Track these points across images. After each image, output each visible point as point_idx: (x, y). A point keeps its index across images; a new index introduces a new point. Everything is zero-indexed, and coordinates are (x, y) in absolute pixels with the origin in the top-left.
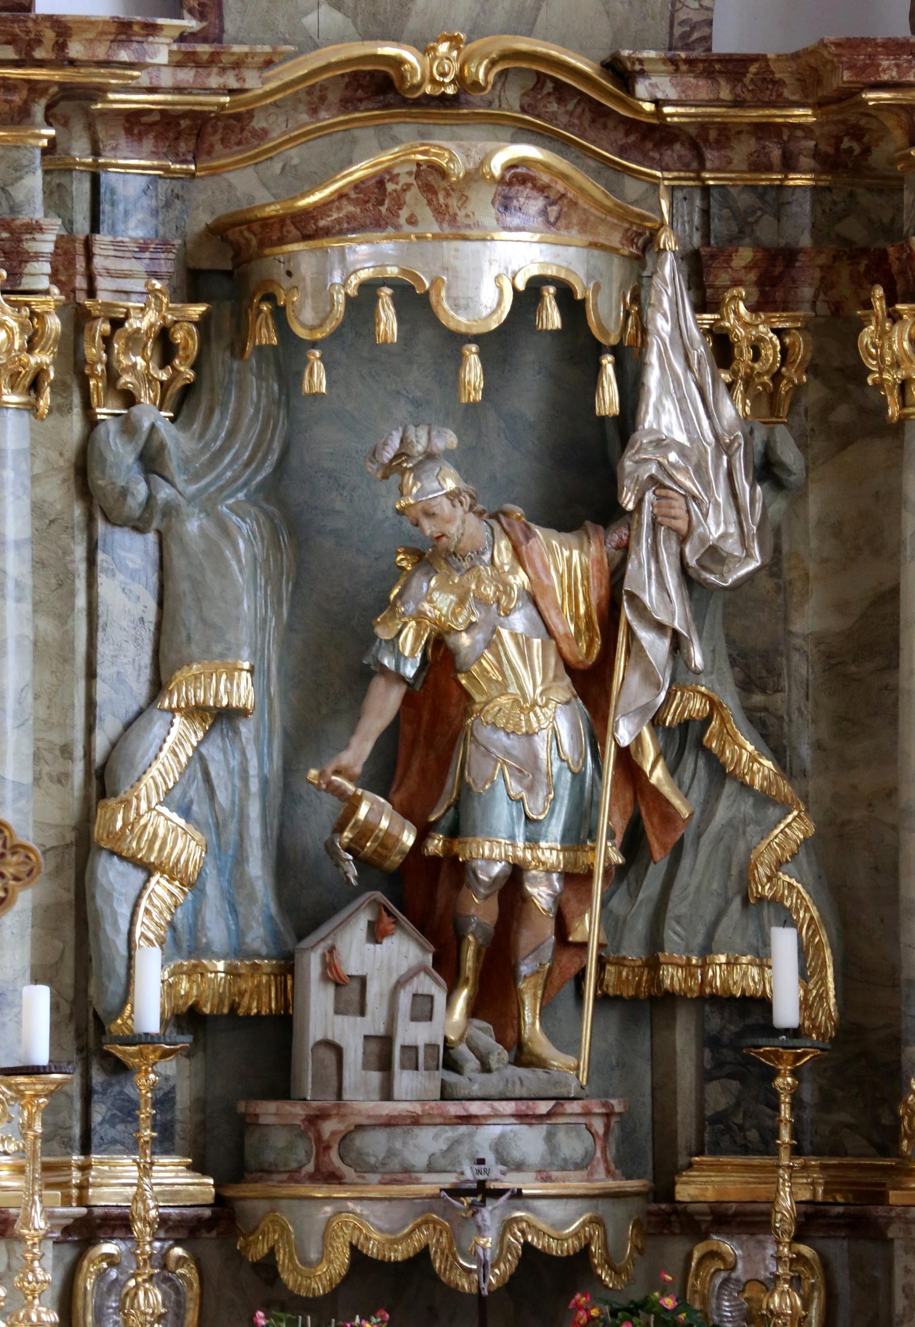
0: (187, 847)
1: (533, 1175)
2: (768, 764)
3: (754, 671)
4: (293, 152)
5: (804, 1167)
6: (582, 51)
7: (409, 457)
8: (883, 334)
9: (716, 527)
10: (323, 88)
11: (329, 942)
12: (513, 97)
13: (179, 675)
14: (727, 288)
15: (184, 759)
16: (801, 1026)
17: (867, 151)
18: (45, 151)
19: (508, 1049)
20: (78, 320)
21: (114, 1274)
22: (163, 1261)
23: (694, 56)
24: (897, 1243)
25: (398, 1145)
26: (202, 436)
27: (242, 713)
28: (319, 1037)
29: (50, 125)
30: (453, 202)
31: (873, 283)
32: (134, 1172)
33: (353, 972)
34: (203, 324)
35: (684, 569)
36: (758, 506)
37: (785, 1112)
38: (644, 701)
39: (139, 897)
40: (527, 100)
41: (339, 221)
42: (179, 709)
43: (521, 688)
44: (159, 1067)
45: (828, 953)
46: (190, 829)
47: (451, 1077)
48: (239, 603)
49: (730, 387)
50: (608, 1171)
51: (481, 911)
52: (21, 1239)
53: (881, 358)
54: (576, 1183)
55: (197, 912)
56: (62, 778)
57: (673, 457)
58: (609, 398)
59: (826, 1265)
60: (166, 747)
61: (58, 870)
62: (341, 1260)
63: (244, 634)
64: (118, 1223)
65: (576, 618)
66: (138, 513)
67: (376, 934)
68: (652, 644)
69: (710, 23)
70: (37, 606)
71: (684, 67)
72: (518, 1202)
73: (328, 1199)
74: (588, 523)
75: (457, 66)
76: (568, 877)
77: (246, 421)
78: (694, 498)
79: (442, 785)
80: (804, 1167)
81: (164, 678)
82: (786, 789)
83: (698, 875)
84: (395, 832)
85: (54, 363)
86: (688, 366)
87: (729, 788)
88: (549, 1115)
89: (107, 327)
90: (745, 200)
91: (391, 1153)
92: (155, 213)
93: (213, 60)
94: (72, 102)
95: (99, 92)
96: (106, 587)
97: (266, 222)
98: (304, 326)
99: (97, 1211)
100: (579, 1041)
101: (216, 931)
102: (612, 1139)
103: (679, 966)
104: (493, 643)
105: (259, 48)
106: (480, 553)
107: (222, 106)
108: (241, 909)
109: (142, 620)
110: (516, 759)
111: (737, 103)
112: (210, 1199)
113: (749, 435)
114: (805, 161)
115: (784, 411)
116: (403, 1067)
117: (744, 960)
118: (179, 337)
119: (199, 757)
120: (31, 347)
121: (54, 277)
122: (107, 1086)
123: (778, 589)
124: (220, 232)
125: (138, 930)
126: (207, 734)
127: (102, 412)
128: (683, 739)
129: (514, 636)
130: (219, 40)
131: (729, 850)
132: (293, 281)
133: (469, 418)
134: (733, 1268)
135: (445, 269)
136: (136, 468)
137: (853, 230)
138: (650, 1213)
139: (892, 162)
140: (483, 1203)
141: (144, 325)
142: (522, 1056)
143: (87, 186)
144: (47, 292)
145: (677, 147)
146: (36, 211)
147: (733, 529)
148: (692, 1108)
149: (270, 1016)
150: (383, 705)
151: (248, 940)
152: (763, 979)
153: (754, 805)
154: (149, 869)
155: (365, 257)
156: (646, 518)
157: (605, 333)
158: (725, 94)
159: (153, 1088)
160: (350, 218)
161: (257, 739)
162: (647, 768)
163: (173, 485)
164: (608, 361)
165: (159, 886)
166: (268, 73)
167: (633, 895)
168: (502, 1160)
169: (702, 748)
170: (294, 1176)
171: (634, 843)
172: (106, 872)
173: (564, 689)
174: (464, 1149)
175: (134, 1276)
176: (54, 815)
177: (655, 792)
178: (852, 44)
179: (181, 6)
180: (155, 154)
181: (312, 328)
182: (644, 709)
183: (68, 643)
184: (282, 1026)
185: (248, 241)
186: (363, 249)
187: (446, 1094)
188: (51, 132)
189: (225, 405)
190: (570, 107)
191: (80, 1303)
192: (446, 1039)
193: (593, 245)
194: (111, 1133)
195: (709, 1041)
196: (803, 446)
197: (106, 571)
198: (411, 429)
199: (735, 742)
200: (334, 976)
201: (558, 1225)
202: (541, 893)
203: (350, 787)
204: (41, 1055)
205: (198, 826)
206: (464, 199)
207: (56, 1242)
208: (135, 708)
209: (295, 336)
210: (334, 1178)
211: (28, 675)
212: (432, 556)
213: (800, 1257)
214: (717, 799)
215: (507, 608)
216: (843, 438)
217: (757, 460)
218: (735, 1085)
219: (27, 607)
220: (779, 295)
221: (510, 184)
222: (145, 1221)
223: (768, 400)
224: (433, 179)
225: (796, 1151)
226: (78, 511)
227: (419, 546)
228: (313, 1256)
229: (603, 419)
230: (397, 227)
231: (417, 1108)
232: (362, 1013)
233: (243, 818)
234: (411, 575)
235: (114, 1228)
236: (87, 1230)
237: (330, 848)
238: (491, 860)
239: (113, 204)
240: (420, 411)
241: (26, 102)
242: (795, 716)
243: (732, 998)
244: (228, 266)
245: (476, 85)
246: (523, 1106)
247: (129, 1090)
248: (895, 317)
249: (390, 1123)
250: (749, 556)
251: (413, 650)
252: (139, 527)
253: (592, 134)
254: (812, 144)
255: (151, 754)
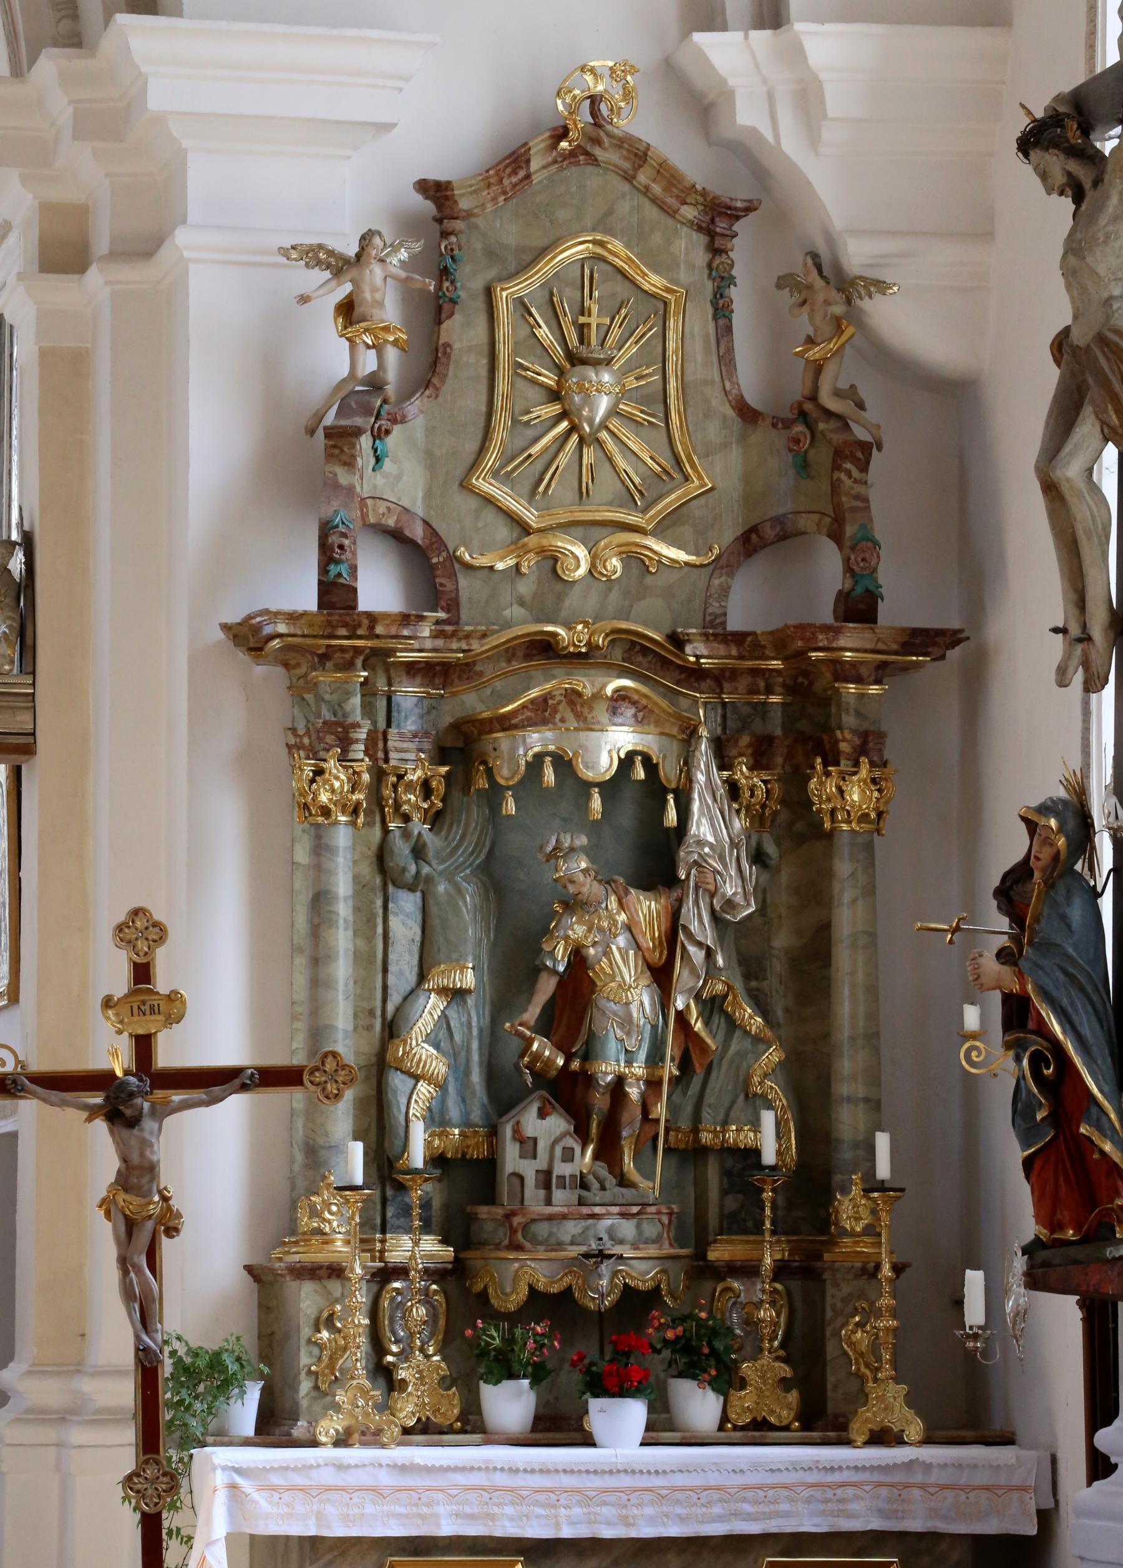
0: (439, 1067)
1: (628, 1247)
2: (759, 1020)
3: (751, 968)
4: (497, 684)
5: (778, 1241)
6: (656, 629)
7: (561, 850)
8: (821, 783)
9: (730, 889)
10: (514, 648)
11: (516, 1118)
12: (618, 654)
13: (434, 971)
14: (736, 757)
15: (436, 1017)
16: (777, 1164)
17: (811, 684)
18: (362, 684)
19: (615, 1177)
20: (379, 775)
21: (399, 1298)
22: (426, 1292)
23: (716, 632)
24: (828, 1282)
25: (555, 1230)
26: (446, 838)
27: (468, 991)
28: (511, 1171)
29: (365, 670)
30: (586, 710)
31: (816, 755)
32: (410, 1244)
33: (530, 1136)
34: (447, 777)
35: (713, 912)
36: (754, 877)
37: (768, 1212)
38: (691, 984)
39: (412, 1093)
40: (626, 655)
41: (522, 721)
42: (433, 989)
43: (623, 978)
44: (422, 1187)
45: (792, 1124)
46: (440, 1056)
47: (584, 1193)
48: (467, 931)
49: (738, 811)
50: (671, 1245)
51: (600, 1102)
52: (349, 1279)
53: (820, 797)
54: (652, 1251)
55: (443, 1101)
56: (370, 1028)
57: (707, 850)
58: (671, 816)
59: (789, 1293)
60: (426, 1010)
61: (367, 1079)
62: (523, 1293)
63: (469, 948)
64: (401, 1272)
65: (653, 939)
66: (411, 881)
67: (542, 1114)
68: (695, 953)
69: (725, 614)
70: (356, 933)
71: (711, 638)
72: (620, 1261)
73: (517, 1259)
74: (660, 887)
75: (587, 637)
76: (648, 1083)
77: (471, 829)
78: (718, 872)
79: (579, 1031)
80: (778, 1241)
81: (425, 971)
82: (769, 1033)
83: (720, 1080)
84: (553, 1058)
85: (366, 799)
86: (715, 800)
87: (738, 1033)
88: (638, 1213)
89: (395, 779)
90: (745, 710)
91: (551, 1235)
92: (421, 717)
93: (454, 634)
94: (378, 658)
95: (392, 652)
96: (394, 922)
97: (482, 722)
98: (503, 778)
99: (390, 1265)
100: (655, 1173)
101: (454, 1112)
102: (672, 1228)
103: (710, 1132)
104: (607, 953)
105: (479, 628)
106: (600, 903)
107: (459, 659)
108: (468, 1101)
109: (413, 940)
110: (620, 1017)
111: (741, 657)
112: (451, 1259)
113: (748, 838)
114: (778, 689)
115: (768, 824)
116: (557, 1187)
117: (746, 1128)
118: (434, 784)
119: (444, 1015)
120: (353, 790)
121: (366, 752)
122: (395, 1197)
123: (765, 923)
124: (457, 727)
125: (411, 1112)
126: (449, 1003)
127: (392, 826)
128: (712, 1006)
129: (619, 949)
130: (457, 623)
131: (738, 1068)
132: (497, 753)
133: (594, 828)
134: (739, 1296)
135: (581, 747)
136: (410, 856)
137: (804, 726)
138: (693, 1267)
139: (825, 690)
140: (602, 1262)
141: (415, 778)
142: (623, 1181)
143: (385, 702)
144: (362, 760)
145: (708, 681)
146: (357, 716)
147: (739, 890)
148: (717, 1210)
149: (484, 1159)
150: (546, 987)
151: (472, 1117)
152: (756, 1138)
153: (752, 1043)
154: (417, 1078)
155: (537, 740)
156: (692, 884)
157: (669, 781)
158: (734, 652)
159: (420, 1198)
160: (528, 719)
161: (476, 1006)
162: (693, 1022)
163: (430, 865)
164: (671, 798)
165: (423, 1088)
166: (485, 641)
167: (685, 1093)
168: (612, 1238)
169: (723, 1011)
170: (497, 1247)
171: (685, 1063)
172: (393, 1080)
173: (646, 979)
174: (591, 1233)
175: (410, 1300)
176: (366, 1048)
177: (696, 1035)
178: (801, 627)
179: (437, 605)
180: (421, 685)
181: (507, 779)
182: (690, 990)
183: (373, 954)
184: (490, 1166)
185: (472, 732)
186: (536, 735)
187: (581, 1202)
188: (366, 674)
189: (459, 822)
190: (650, 658)
191: (381, 1314)
192: (581, 1172)
193: (662, 734)
194: (397, 1222)
195: (726, 1173)
196: (778, 844)
197: (393, 913)
198: (562, 835)
199: (741, 1007)
200: (519, 1137)
201: (643, 1272)
202: (634, 1092)
203: (528, 1033)
204: (359, 1180)
205: (444, 1054)
206: (591, 709)
207: (368, 1281)
208: (409, 989)
209: (498, 784)
210: (519, 1248)
211: (351, 971)
212: (574, 904)
213: (775, 1290)
214: (731, 1039)
215: (615, 935)
216: (801, 840)
217: (753, 852)
218: (740, 1196)
219: (350, 933)
220: (765, 761)
221: (616, 700)
222: (416, 1270)
223: (759, 819)
224: (574, 697)
225: (773, 1233)
226: (378, 880)
227: (566, 899)
228: (508, 1290)
229: (668, 828)
230: (554, 724)
231: (565, 1210)
232: (535, 1158)
233: (469, 1050)
234: (562, 915)
235: (399, 1274)
236: (384, 1275)
237: (517, 1067)
238: (606, 1073)
239: (399, 712)
240: (567, 824)
241: (352, 658)
242: (774, 993)
243: (739, 1149)
244: (460, 744)
245: (598, 647)
246: (624, 1209)
247: (407, 1199)
248: (828, 774)
249: (550, 1218)
250: (749, 905)
251: (563, 957)
252: (412, 889)
253: (661, 674)
254: (781, 680)
255: (418, 1014)
